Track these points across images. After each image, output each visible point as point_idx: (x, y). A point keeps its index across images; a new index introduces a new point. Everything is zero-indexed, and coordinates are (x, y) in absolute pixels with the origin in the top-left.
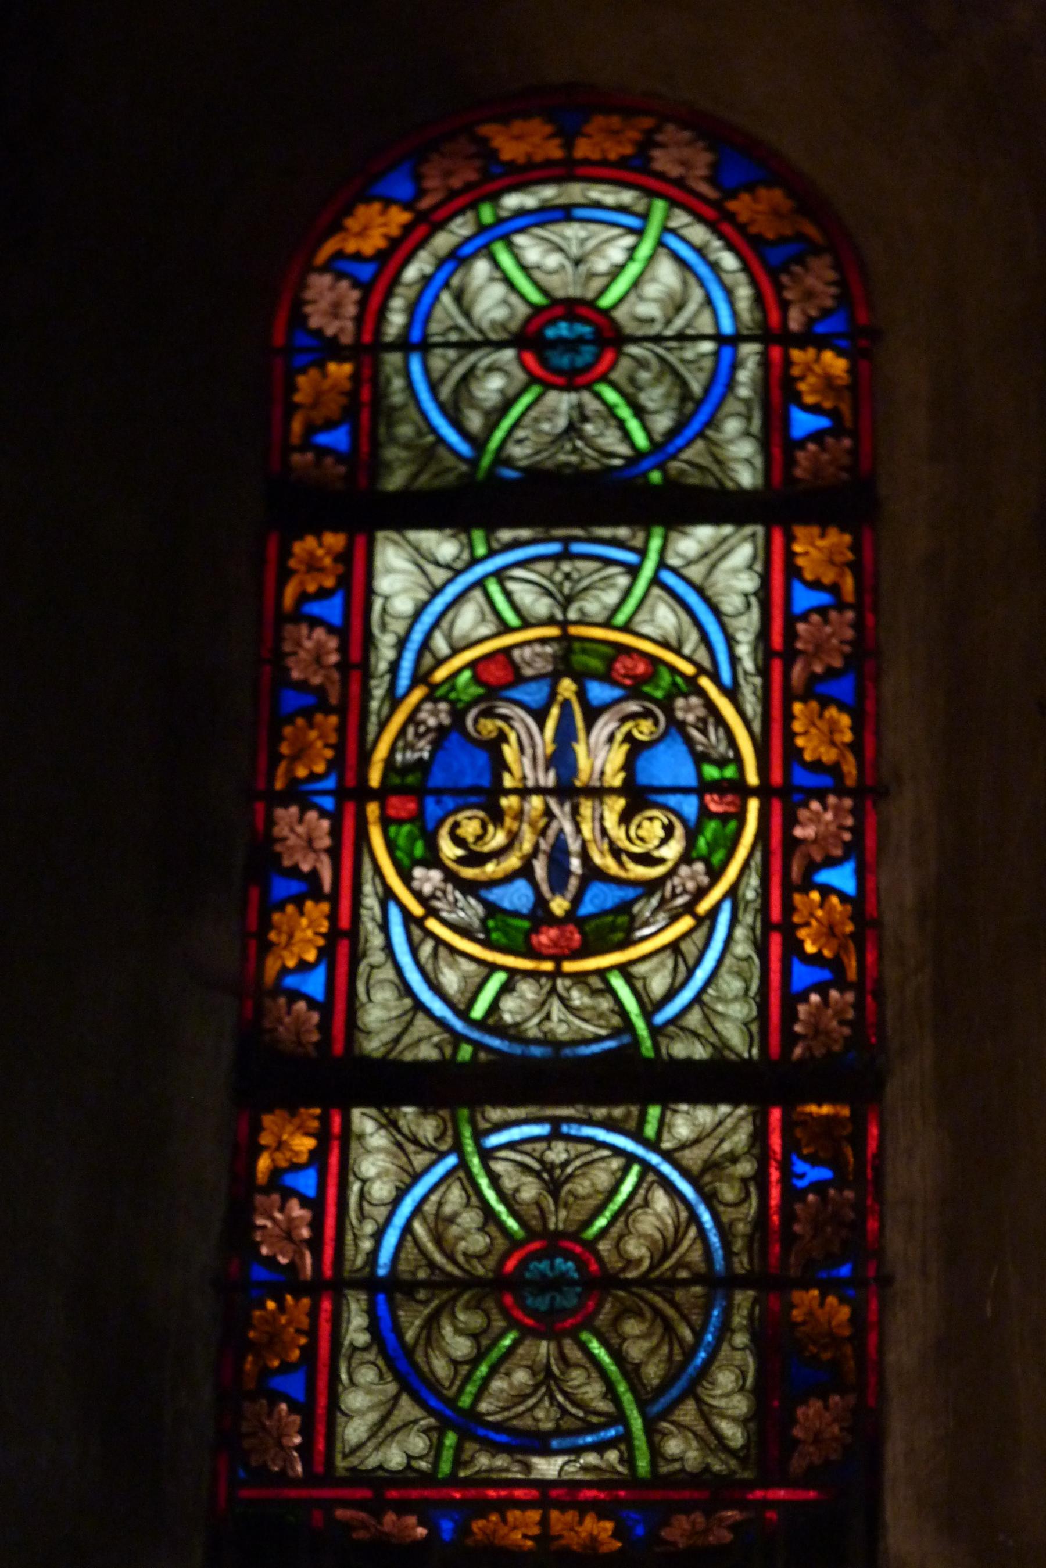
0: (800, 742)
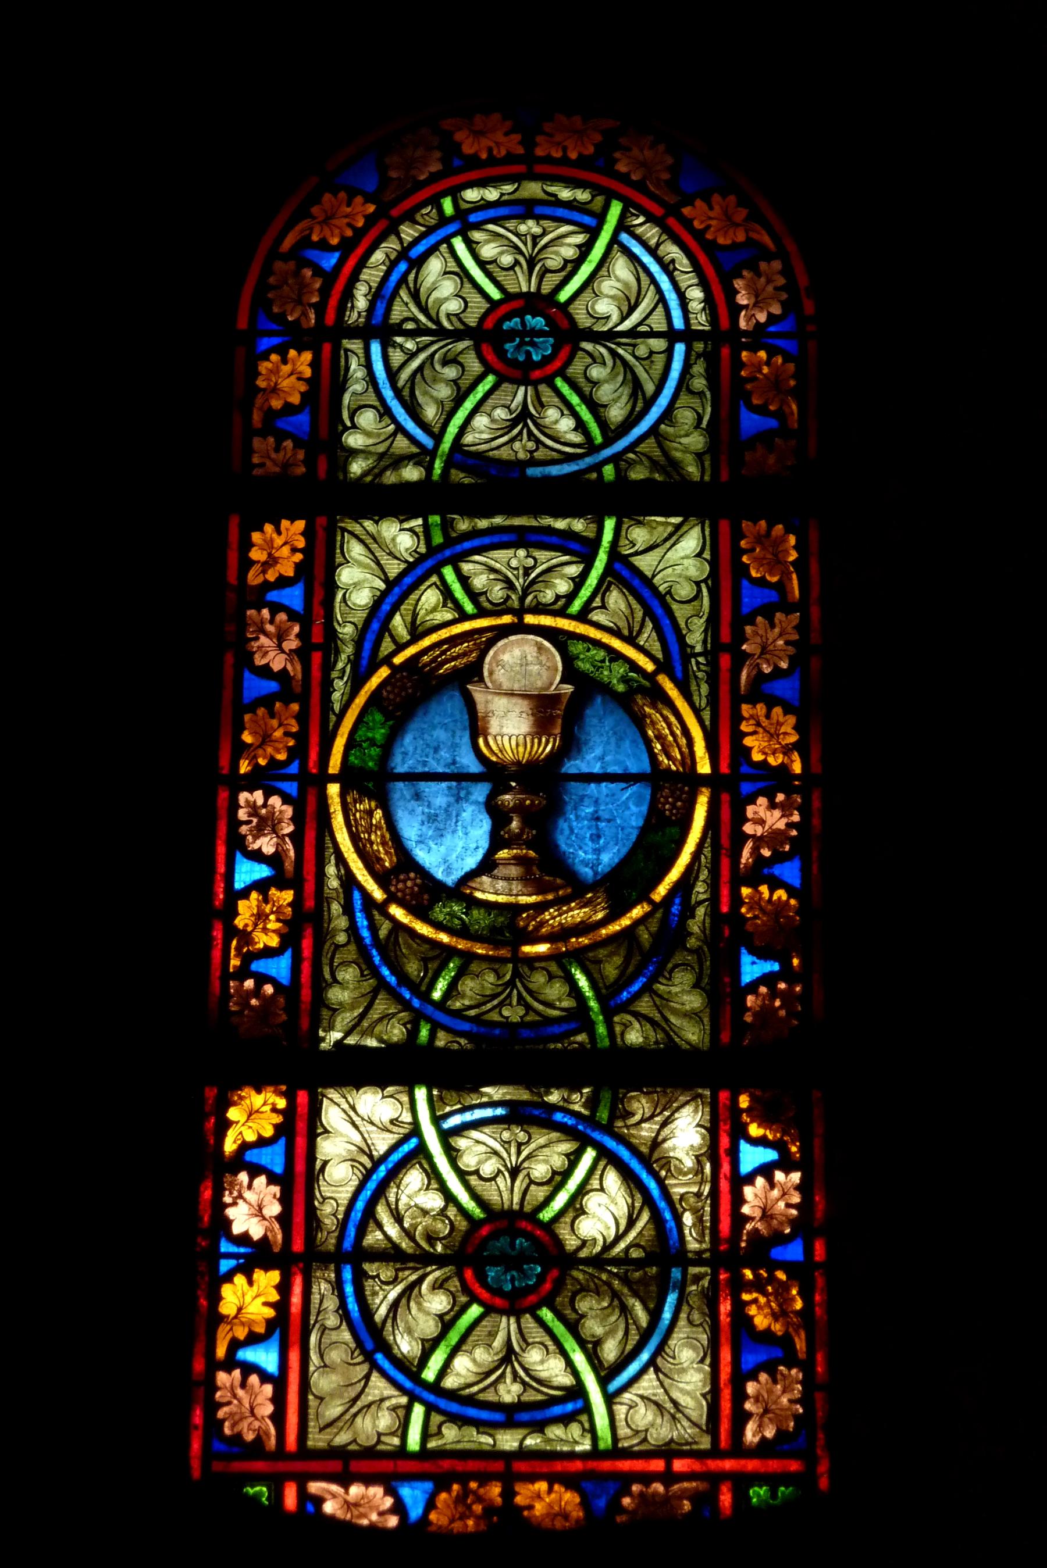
0: (748, 741)
